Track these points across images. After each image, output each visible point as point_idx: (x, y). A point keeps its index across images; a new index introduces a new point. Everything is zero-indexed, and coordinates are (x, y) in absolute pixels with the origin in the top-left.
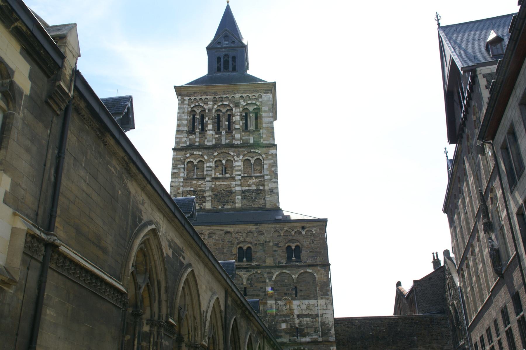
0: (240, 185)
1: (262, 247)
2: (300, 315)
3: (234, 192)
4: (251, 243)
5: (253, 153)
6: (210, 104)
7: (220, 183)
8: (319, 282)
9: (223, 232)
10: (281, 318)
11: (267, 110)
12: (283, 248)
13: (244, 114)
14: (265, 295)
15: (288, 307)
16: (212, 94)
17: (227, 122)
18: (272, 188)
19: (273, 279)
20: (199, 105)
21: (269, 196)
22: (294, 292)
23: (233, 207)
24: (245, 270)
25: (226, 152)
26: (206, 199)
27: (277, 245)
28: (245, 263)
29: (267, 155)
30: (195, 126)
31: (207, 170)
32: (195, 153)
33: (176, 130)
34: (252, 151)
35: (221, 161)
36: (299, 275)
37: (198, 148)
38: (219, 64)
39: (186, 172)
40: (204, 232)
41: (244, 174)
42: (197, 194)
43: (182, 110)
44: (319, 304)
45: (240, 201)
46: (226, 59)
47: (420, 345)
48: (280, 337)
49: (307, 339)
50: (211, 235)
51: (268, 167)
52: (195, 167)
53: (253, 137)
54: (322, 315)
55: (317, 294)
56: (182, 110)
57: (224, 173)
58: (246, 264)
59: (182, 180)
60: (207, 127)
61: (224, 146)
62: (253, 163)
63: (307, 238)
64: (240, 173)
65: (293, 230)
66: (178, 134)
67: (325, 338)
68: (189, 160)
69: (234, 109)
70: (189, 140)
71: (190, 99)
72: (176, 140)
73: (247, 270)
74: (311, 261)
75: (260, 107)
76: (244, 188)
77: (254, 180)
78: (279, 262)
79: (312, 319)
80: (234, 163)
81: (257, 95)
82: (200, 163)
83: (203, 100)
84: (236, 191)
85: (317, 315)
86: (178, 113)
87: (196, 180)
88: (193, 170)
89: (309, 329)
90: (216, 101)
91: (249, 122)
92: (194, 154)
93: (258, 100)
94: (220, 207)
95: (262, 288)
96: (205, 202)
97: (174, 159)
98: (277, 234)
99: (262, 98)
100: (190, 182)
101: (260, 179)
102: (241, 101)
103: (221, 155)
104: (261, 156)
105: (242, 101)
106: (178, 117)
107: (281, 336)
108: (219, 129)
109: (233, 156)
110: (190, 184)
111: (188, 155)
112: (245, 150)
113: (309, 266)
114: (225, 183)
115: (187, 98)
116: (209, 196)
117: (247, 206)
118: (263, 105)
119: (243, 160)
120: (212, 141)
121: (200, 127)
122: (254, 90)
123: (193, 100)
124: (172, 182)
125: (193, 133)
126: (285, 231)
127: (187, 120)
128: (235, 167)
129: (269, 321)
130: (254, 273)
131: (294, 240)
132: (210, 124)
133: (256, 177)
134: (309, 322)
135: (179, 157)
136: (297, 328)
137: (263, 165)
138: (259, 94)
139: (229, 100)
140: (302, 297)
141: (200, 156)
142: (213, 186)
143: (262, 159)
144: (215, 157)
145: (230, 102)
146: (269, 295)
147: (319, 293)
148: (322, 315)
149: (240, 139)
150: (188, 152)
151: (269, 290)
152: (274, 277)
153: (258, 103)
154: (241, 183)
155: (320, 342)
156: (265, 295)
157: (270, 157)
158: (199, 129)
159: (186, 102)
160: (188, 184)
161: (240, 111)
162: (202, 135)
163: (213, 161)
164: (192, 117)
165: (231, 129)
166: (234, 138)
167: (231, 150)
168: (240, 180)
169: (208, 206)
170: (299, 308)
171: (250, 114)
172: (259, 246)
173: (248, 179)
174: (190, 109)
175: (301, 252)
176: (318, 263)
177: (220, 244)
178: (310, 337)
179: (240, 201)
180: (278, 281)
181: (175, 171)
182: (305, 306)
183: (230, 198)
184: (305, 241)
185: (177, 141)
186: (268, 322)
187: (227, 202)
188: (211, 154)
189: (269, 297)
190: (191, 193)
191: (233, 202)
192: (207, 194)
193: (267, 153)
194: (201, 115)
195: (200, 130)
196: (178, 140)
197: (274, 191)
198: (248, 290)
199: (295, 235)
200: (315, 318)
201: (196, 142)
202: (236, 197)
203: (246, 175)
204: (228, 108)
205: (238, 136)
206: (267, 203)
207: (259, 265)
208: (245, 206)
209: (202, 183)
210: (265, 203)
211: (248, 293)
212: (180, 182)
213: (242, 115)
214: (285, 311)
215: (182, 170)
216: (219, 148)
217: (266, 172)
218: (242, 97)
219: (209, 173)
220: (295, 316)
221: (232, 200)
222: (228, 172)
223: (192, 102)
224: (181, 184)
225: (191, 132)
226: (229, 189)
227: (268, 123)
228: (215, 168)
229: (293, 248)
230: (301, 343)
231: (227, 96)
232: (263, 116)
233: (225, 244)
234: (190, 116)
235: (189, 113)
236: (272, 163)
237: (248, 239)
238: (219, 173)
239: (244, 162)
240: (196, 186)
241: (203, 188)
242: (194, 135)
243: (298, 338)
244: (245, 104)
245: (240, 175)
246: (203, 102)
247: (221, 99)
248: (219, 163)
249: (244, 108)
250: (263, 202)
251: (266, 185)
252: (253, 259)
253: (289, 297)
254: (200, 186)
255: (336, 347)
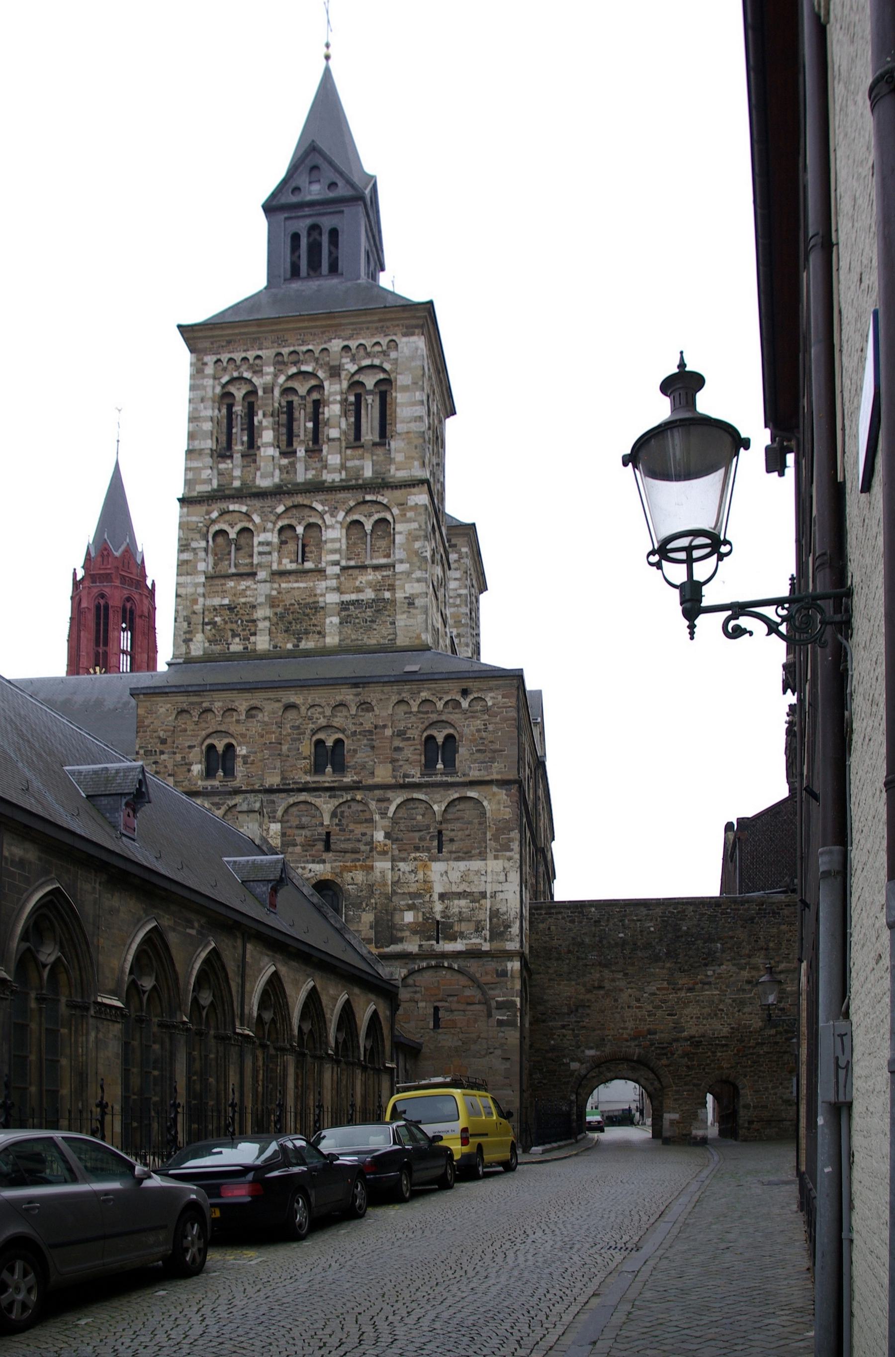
0: (338, 590)
1: (368, 740)
2: (446, 893)
3: (322, 608)
4: (343, 731)
5: (369, 504)
6: (268, 374)
7: (290, 585)
8: (493, 819)
9: (280, 705)
10: (403, 900)
11: (409, 382)
12: (416, 742)
13: (352, 398)
14: (371, 850)
15: (421, 875)
16: (273, 342)
17: (310, 421)
18: (412, 595)
19: (390, 814)
20: (241, 378)
21: (404, 616)
22: (435, 843)
23: (320, 644)
24: (328, 794)
25: (305, 503)
26: (256, 626)
27: (401, 734)
28: (328, 777)
29: (403, 510)
30: (234, 437)
31: (260, 553)
32: (231, 508)
33: (185, 447)
34: (368, 498)
35: (292, 527)
36: (402, 803)
37: (239, 495)
38: (297, 254)
39: (211, 560)
40: (236, 704)
41: (349, 559)
42: (236, 615)
43: (200, 393)
44: (489, 870)
45: (335, 628)
46: (315, 239)
47: (728, 960)
48: (401, 940)
49: (459, 946)
50: (254, 712)
51: (404, 541)
52: (233, 546)
53: (373, 461)
54: (494, 895)
55: (486, 847)
56: (200, 393)
57: (300, 560)
58: (329, 779)
59: (202, 579)
60: (260, 436)
61: (301, 487)
62: (369, 532)
63: (473, 717)
64: (336, 557)
65: (440, 699)
66: (191, 460)
67: (497, 945)
68: (216, 527)
69: (326, 384)
70: (219, 474)
71: (219, 360)
72: (186, 474)
73: (333, 793)
74: (477, 773)
75: (393, 376)
76: (347, 597)
77: (371, 576)
78: (406, 776)
79: (472, 902)
80: (323, 532)
81: (384, 341)
82: (246, 535)
83: (251, 361)
84: (326, 604)
85: (483, 895)
86: (190, 401)
87: (235, 578)
88: (229, 553)
89: (463, 924)
90: (284, 363)
91: (363, 420)
92: (229, 512)
93: (389, 355)
94: (290, 646)
95: (364, 834)
96: (255, 634)
97: (181, 526)
98: (403, 708)
99: (397, 350)
100: (222, 585)
101: (385, 573)
102: (344, 360)
103: (294, 511)
104: (390, 510)
105: (348, 360)
106: (189, 412)
107: (403, 938)
108: (290, 443)
109: (321, 515)
110: (219, 588)
111: (215, 515)
112: (350, 495)
113: (472, 784)
114: (302, 585)
115: (210, 359)
116: (265, 619)
117: (352, 641)
118: (398, 371)
119: (345, 525)
120: (273, 476)
121: (245, 438)
122: (377, 328)
123: (225, 364)
124: (178, 584)
125: (228, 454)
126: (423, 701)
127: (212, 419)
128: (326, 542)
129: (378, 905)
130: (347, 801)
131: (442, 721)
132: (267, 428)
133: (376, 568)
134: (464, 910)
135: (194, 519)
136: (438, 922)
137: (394, 534)
138: (390, 338)
139: (317, 360)
140: (454, 855)
141: (243, 515)
142: (274, 593)
143: (391, 520)
144: (279, 516)
145: (317, 363)
146: (379, 849)
147: (491, 844)
148: (494, 895)
149: (339, 467)
150: (214, 506)
151: (379, 836)
152: (392, 808)
153: (387, 366)
154: (340, 583)
155: (486, 952)
156: (371, 850)
157: (410, 514)
158: (242, 443)
159: (209, 370)
160: (215, 589)
161: (341, 389)
162: (249, 459)
163: (274, 527)
164: (224, 411)
165: (320, 442)
166: (325, 467)
167: (318, 498)
168: (338, 577)
169: (262, 643)
170: (445, 878)
171: (367, 397)
172: (361, 737)
173: (356, 572)
174: (218, 390)
175: (458, 752)
176: (495, 777)
177: (274, 732)
178: (465, 942)
179: (335, 630)
180: (401, 818)
181: (186, 556)
182: (459, 874)
183: (314, 621)
184: (468, 726)
185: (188, 477)
186: (376, 908)
187: (307, 632)
188: (270, 509)
189: (379, 853)
190: (222, 612)
191: (319, 633)
192: (260, 613)
193: (402, 504)
194: (246, 404)
195: (246, 445)
196: (190, 476)
197: (416, 601)
198: (333, 839)
199: (446, 710)
200: (478, 902)
201: (233, 478)
202: (328, 621)
203: (352, 563)
204: (313, 382)
205: (334, 460)
206: (398, 632)
207: (360, 782)
208: (348, 641)
209: (249, 587)
210: (395, 634)
211: (332, 846)
212: (196, 585)
213: (346, 400)
214: (412, 885)
215: (202, 554)
216: (290, 493)
217: (399, 554)
218: (346, 348)
219: (265, 559)
220: (436, 897)
221: (319, 628)
222: (309, 555)
223: (225, 369)
224: (201, 590)
225: (223, 452)
226: (311, 600)
227: (410, 422)
228: (281, 547)
229: (440, 739)
230: (444, 955)
231: (310, 347)
232: (398, 401)
233: (284, 733)
234: (220, 410)
235: (217, 399)
236: (415, 529)
237: (337, 722)
238: (288, 560)
239: (348, 528)
240: (235, 595)
241: (251, 599)
242: (229, 461)
243: (438, 943)
244: (353, 368)
245: (336, 563)
246: (251, 367)
247: (294, 358)
248: (288, 534)
249: (352, 380)
250: (391, 631)
251: (397, 587)
252: (348, 767)
253: (424, 855)
254: (243, 593)
255: (519, 963)
